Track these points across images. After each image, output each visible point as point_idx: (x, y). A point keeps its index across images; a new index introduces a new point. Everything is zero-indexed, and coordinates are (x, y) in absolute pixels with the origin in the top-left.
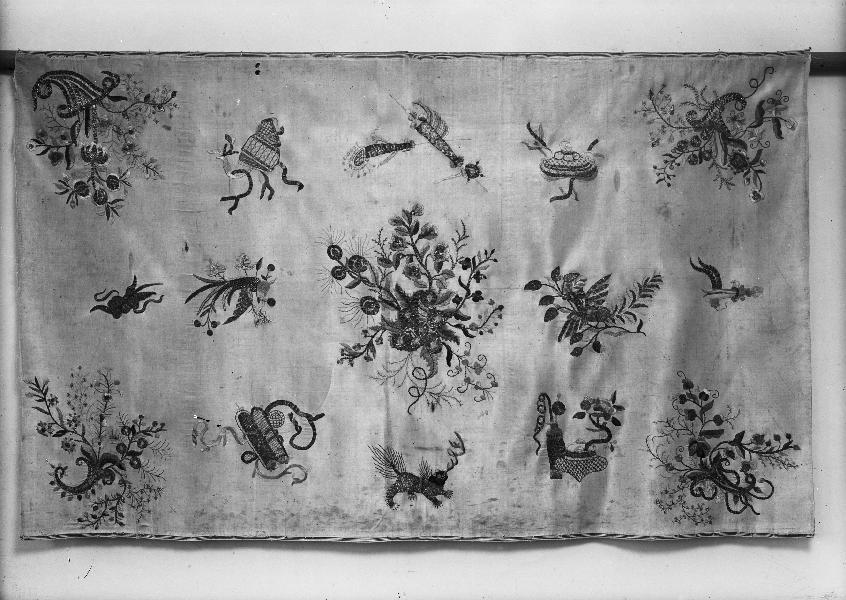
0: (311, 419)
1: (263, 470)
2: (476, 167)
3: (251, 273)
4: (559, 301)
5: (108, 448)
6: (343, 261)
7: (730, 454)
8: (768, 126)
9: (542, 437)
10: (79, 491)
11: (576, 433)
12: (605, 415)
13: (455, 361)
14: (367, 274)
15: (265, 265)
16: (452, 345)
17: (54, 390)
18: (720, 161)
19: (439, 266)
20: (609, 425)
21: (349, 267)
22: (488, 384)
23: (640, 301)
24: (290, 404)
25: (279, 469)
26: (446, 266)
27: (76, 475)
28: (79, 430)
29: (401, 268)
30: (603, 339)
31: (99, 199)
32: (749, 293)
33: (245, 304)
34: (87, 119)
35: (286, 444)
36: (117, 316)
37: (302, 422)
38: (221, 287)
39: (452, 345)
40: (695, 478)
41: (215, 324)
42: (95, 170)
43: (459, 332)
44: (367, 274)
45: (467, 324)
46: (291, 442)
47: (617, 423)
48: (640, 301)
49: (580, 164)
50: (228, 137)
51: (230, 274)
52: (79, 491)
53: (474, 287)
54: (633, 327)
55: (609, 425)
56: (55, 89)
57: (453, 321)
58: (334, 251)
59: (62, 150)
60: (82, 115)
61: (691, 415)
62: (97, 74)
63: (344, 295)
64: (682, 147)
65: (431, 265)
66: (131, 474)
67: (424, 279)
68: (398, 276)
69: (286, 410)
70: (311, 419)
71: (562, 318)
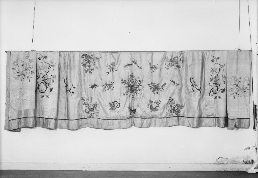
0: (119, 104)
1: (112, 111)
2: (141, 67)
3: (111, 83)
4: (152, 87)
5: (92, 107)
6: (123, 81)
7: (176, 107)
8: (181, 61)
9: (149, 106)
10: (88, 113)
11: (154, 105)
12: (158, 104)
13: (138, 94)
14: (126, 83)
15: (113, 82)
16: (137, 92)
17: (85, 99)
18: (175, 66)
19: (136, 81)
20: (159, 104)
21: (124, 82)
22: (142, 97)
23: (163, 86)
24: (116, 102)
25: (115, 111)
26: (137, 81)
27: (88, 110)
28: (88, 104)
29: (131, 82)
30: (158, 92)
31: (90, 72)
32: (247, 149)
33: (110, 87)
34: (88, 61)
35: (116, 107)
36: (92, 88)
37: (118, 104)
38: (107, 85)
39: (137, 92)
40: (171, 110)
41: (106, 90)
42: (89, 68)
43: (138, 90)
44: (126, 83)
45: (139, 89)
46: (116, 107)
47: (160, 104)
48: (163, 86)
49: (182, 94)
50: (107, 64)
51: (108, 83)
52: (88, 113)
53: (140, 84)
54: (162, 90)
55: (159, 104)
56: (85, 57)
57: (137, 88)
58: (122, 79)
59: (85, 65)
60: (88, 60)
61: (170, 102)
62: (89, 54)
63: (124, 86)
64: (169, 64)
65: (134, 81)
66: (95, 110)
67: (133, 83)
68: (131, 83)
69: (116, 102)
70: (119, 104)
71: (152, 89)
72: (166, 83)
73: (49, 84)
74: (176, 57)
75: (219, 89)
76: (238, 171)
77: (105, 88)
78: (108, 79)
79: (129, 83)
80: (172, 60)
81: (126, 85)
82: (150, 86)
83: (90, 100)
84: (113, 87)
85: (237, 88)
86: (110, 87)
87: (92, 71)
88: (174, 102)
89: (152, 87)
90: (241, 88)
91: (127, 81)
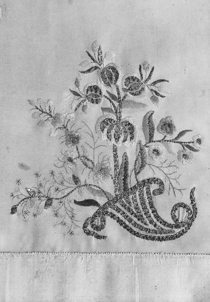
59: (158, 136)
87: (92, 79)
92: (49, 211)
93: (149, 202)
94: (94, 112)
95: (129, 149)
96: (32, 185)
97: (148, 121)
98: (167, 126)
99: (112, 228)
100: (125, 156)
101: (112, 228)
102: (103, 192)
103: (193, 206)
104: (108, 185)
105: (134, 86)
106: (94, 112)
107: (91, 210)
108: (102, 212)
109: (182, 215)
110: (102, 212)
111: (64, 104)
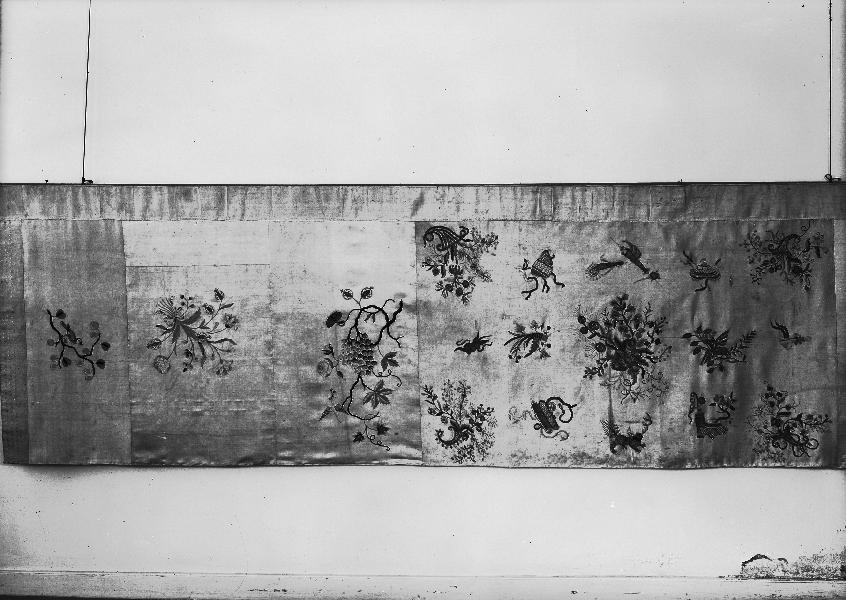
4: (700, 344)
8: (812, 251)
10: (448, 444)
24: (558, 398)
27: (448, 435)
31: (459, 293)
33: (534, 348)
37: (565, 408)
41: (520, 357)
44: (599, 331)
52: (448, 444)
53: (656, 336)
59: (439, 268)
64: (765, 263)
72: (563, 286)
73: (348, 341)
74: (790, 237)
75: (349, 323)
76: (678, 183)
77: (516, 349)
78: (527, 312)
79: (609, 331)
80: (776, 246)
81: (597, 339)
82: (694, 344)
83: (457, 396)
84: (549, 346)
85: (202, 327)
86: (534, 348)
87: (466, 291)
88: (788, 407)
89: (700, 344)
90: (182, 330)
91: (602, 324)
92: (482, 237)
93: (31, 235)
94: (465, 277)
95: (451, 262)
96: (490, 249)
97: (444, 274)
98: (436, 272)
99: (458, 231)
100: (452, 259)
101: (458, 231)
102: (461, 245)
103: (76, 339)
104: (459, 248)
105: (449, 288)
106: (465, 277)
107: (466, 238)
108: (461, 237)
109: (429, 236)
110: (461, 237)
111: (478, 281)
